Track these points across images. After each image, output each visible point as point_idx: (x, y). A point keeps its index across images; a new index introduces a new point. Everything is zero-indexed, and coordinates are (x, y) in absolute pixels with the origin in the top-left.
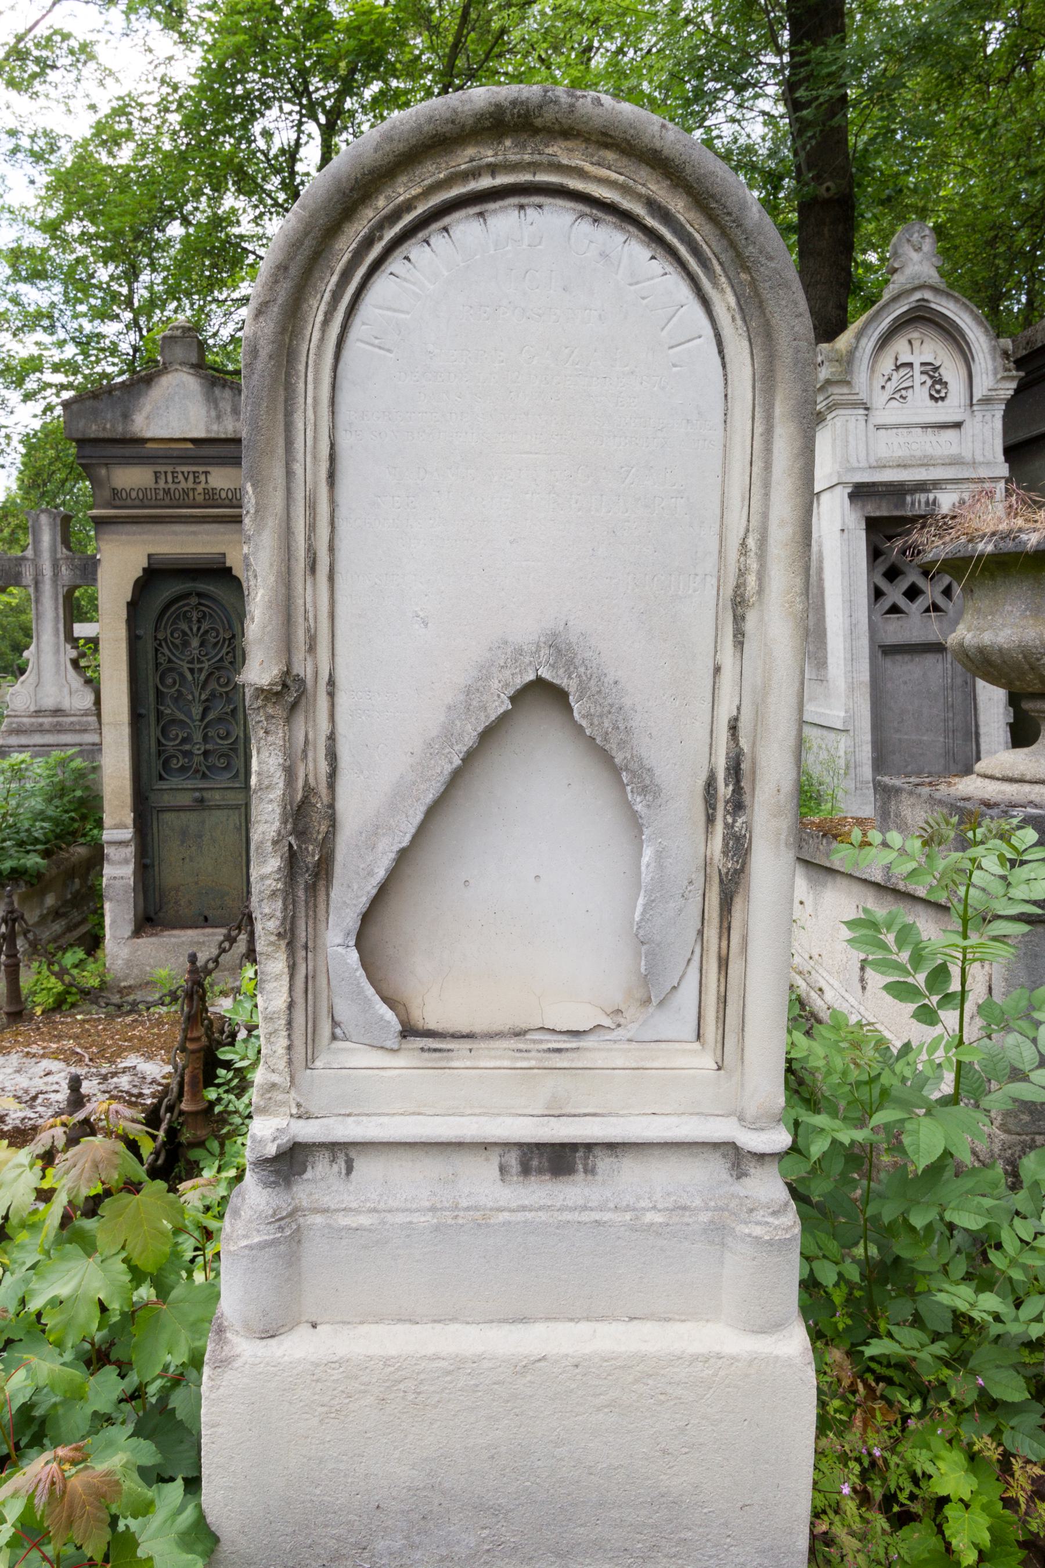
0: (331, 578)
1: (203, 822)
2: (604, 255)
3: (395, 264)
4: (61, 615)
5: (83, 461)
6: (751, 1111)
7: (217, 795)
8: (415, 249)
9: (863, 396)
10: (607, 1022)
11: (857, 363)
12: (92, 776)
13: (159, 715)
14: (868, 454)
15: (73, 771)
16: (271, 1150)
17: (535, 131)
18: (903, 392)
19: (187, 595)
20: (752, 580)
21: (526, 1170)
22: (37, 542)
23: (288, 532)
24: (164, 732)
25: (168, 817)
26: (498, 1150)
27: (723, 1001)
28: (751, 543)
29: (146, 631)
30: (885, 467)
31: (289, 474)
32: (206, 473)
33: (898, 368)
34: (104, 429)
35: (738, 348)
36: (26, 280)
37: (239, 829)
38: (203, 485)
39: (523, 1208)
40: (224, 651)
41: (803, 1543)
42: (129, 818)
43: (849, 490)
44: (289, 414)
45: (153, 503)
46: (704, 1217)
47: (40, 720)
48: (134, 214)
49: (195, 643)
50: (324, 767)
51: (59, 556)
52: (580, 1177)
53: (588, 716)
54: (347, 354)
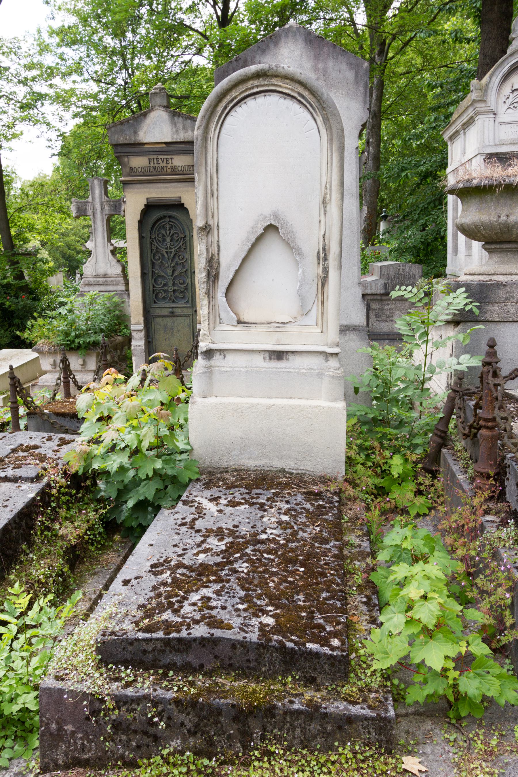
0: (217, 198)
1: (174, 322)
2: (287, 108)
3: (233, 113)
4: (105, 229)
5: (117, 155)
6: (329, 342)
7: (180, 310)
8: (237, 108)
9: (493, 108)
10: (292, 320)
11: (489, 91)
12: (122, 305)
13: (153, 273)
14: (494, 138)
15: (115, 302)
16: (204, 349)
17: (268, 76)
18: (515, 105)
19: (164, 217)
20: (328, 196)
21: (270, 359)
22: (93, 194)
23: (206, 186)
24: (155, 281)
25: (158, 320)
26: (263, 353)
27: (323, 313)
28: (328, 186)
29: (147, 234)
30: (503, 144)
31: (206, 170)
32: (172, 158)
33: (513, 91)
34: (126, 139)
35: (323, 131)
36: (67, 45)
37: (189, 326)
38: (170, 164)
39: (269, 368)
40: (181, 243)
41: (344, 459)
42: (142, 320)
43: (484, 157)
44: (206, 154)
45: (148, 173)
46: (317, 371)
47: (98, 279)
48: (127, 11)
49: (168, 240)
50: (216, 249)
51: (103, 200)
52: (285, 361)
53: (283, 234)
54: (220, 138)
